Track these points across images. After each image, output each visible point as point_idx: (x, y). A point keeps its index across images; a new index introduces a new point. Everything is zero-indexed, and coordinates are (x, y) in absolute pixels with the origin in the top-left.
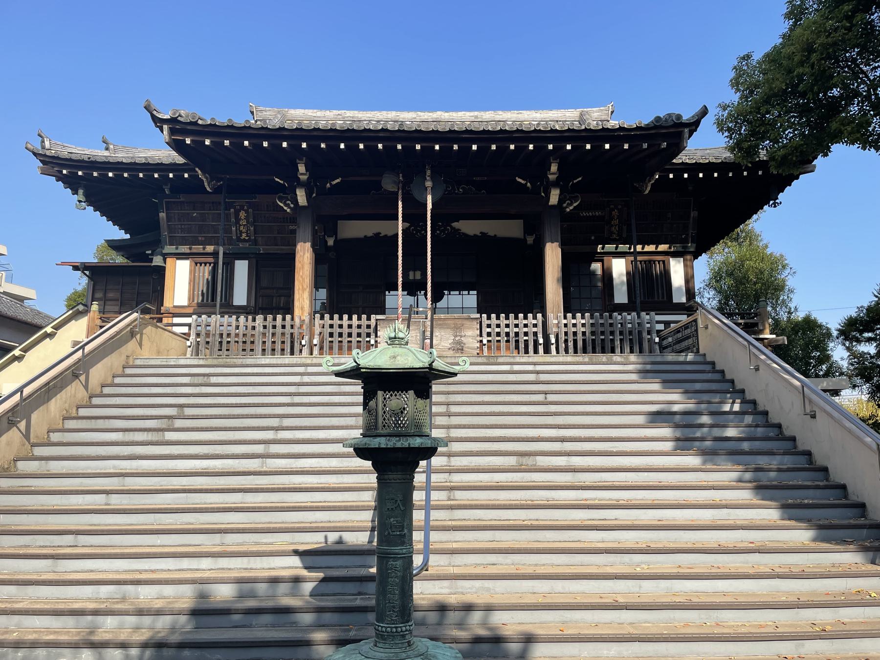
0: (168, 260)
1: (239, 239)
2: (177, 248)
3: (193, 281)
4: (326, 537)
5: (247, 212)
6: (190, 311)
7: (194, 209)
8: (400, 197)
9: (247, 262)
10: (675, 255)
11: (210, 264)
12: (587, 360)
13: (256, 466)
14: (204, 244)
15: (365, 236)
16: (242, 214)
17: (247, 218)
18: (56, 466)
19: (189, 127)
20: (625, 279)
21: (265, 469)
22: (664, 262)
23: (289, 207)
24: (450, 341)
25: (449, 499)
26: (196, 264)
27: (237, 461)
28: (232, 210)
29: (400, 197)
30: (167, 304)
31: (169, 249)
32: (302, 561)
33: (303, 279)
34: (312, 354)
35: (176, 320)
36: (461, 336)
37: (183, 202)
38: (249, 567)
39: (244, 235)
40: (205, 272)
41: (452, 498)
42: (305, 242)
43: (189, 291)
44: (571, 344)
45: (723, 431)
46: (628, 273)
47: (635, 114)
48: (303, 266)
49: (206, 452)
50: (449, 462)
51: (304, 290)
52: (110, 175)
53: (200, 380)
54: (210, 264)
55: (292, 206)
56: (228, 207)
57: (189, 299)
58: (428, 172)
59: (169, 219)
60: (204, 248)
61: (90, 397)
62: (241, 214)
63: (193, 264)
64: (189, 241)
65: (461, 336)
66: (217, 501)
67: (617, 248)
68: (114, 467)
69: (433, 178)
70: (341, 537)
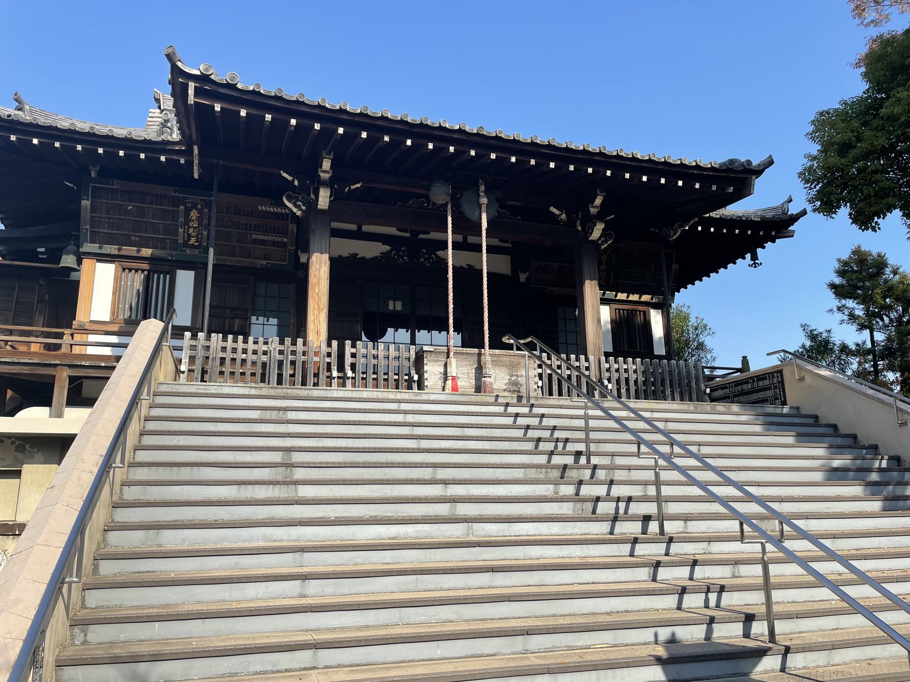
0: (86, 262)
1: (186, 244)
2: (100, 248)
3: (117, 291)
4: (656, 635)
5: (200, 212)
6: (115, 328)
7: (130, 201)
8: (449, 212)
9: (193, 273)
10: (656, 306)
11: (143, 271)
12: (692, 408)
13: (459, 533)
14: (140, 245)
15: (340, 256)
16: (194, 214)
17: (199, 219)
18: (171, 539)
19: (222, 91)
20: (609, 326)
21: (471, 538)
22: (644, 312)
23: (300, 209)
24: (506, 381)
25: (734, 577)
26: (124, 269)
27: (436, 526)
28: (182, 208)
29: (449, 212)
30: (81, 317)
31: (88, 247)
32: (666, 673)
33: (319, 297)
34: (443, 390)
35: (92, 338)
36: (518, 376)
37: (116, 190)
38: (275, 670)
39: (193, 241)
40: (137, 280)
41: (736, 574)
42: (322, 253)
43: (113, 304)
44: (623, 391)
45: (905, 489)
46: (612, 321)
47: (708, 154)
48: (319, 281)
49: (374, 514)
50: (686, 527)
51: (319, 310)
52: (35, 141)
53: (274, 415)
54: (143, 271)
55: (304, 208)
56: (176, 202)
57: (113, 313)
58: (482, 188)
59: (93, 208)
60: (138, 251)
61: (141, 435)
62: (192, 213)
63: (120, 269)
64: (115, 241)
65: (518, 376)
66: (458, 585)
67: (616, 296)
68: (264, 538)
69: (487, 193)
70: (673, 634)
